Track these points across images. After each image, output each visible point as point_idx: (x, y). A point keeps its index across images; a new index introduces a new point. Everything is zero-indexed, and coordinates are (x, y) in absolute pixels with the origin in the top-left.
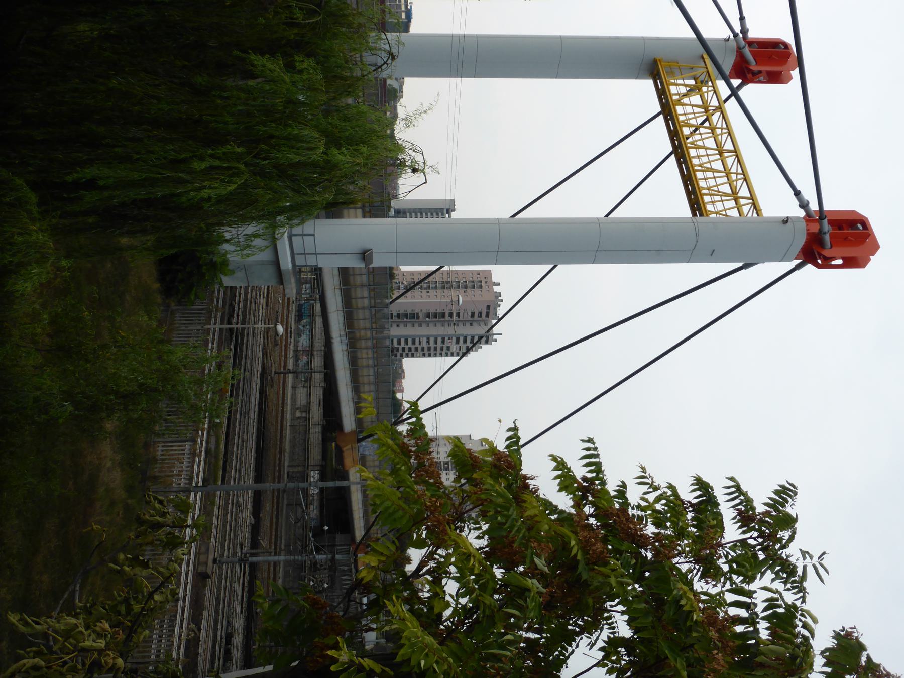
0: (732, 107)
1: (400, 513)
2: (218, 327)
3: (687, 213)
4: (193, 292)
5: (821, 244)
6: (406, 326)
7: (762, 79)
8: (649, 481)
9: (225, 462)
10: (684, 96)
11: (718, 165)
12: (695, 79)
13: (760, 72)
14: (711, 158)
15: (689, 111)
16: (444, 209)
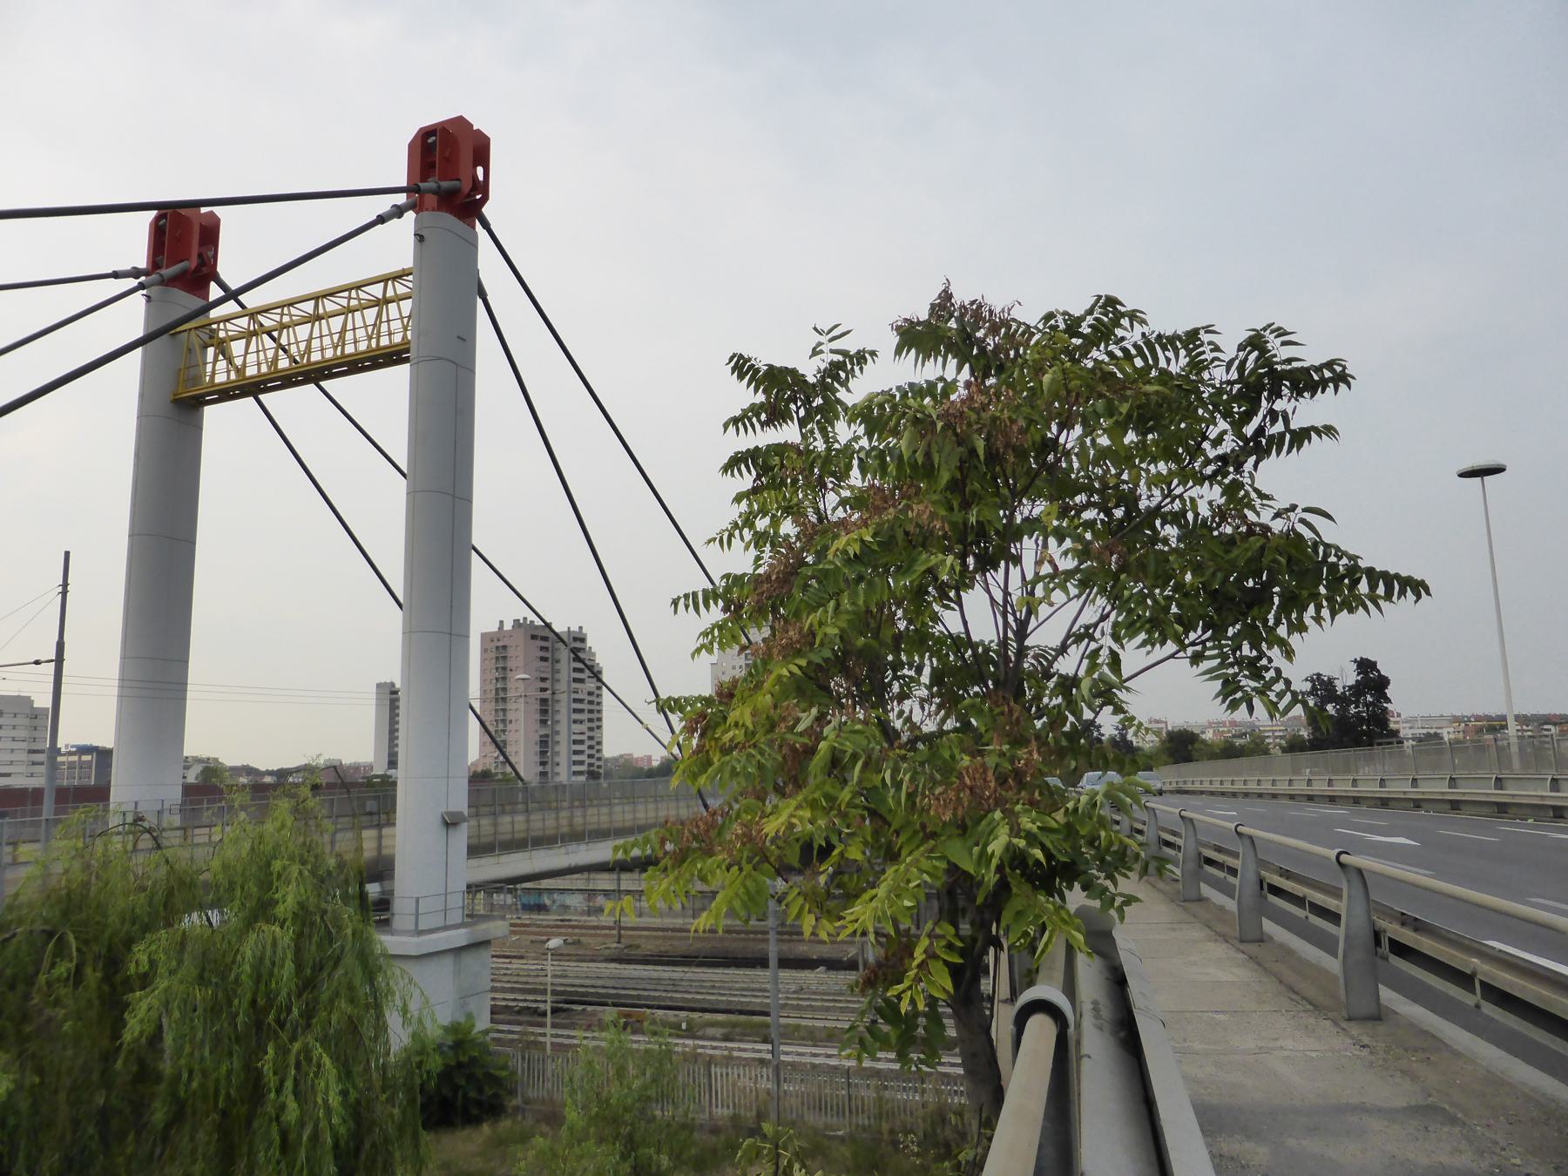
0: (251, 299)
1: (749, 883)
2: (549, 1030)
3: (405, 369)
4: (497, 1073)
5: (454, 192)
6: (558, 753)
7: (210, 254)
8: (726, 535)
9: (741, 1012)
10: (230, 361)
11: (336, 324)
12: (206, 347)
13: (200, 255)
14: (325, 332)
15: (254, 359)
16: (390, 697)
